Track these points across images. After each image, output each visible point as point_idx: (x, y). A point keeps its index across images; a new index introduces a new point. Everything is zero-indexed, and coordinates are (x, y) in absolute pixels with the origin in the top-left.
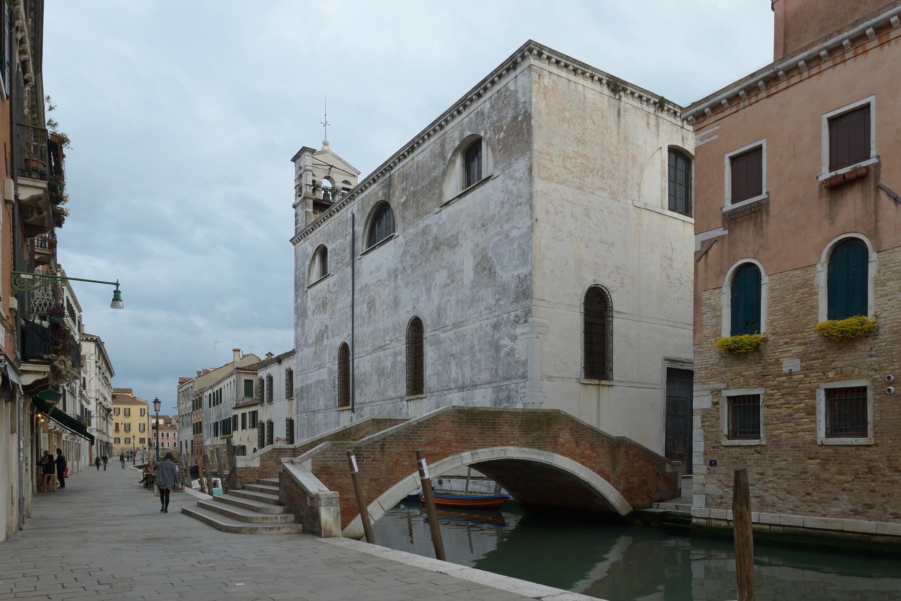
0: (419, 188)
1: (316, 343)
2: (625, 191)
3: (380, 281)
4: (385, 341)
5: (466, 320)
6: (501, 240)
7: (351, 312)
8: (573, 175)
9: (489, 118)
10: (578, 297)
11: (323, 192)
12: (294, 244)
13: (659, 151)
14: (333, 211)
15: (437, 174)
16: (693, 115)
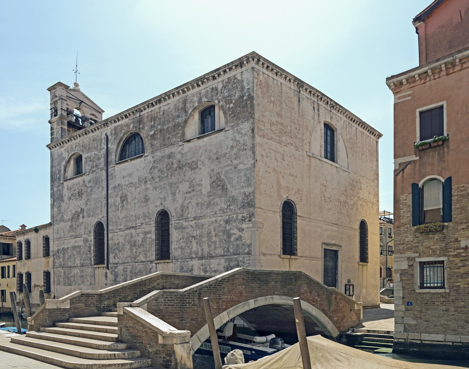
0: (165, 127)
1: (72, 220)
2: (302, 146)
3: (132, 183)
4: (136, 224)
5: (204, 216)
6: (231, 169)
7: (106, 202)
9: (222, 93)
12: (50, 149)
13: (319, 124)
14: (88, 131)
15: (180, 121)
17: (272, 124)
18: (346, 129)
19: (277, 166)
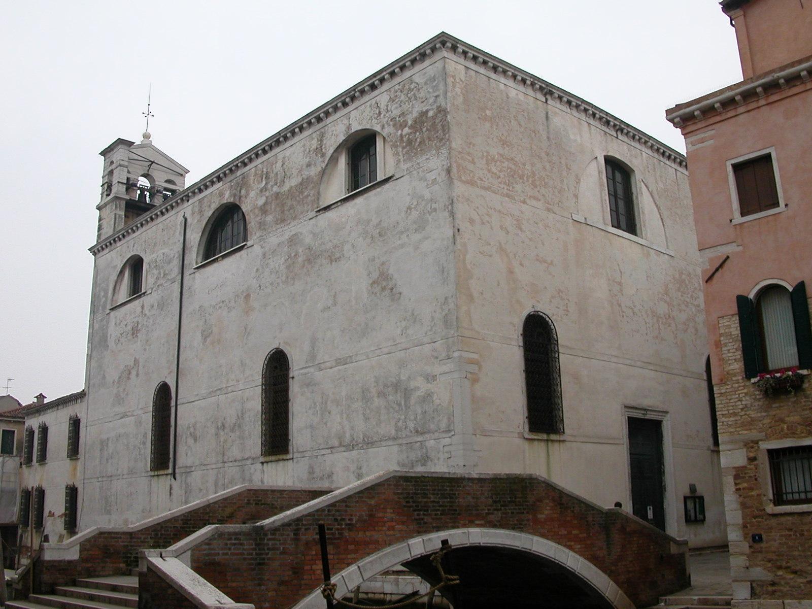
8: (499, 180)
9: (388, 111)
10: (514, 326)
11: (139, 192)
12: (95, 254)
16: (680, 116)
17: (490, 160)
18: (654, 171)
19: (507, 241)
